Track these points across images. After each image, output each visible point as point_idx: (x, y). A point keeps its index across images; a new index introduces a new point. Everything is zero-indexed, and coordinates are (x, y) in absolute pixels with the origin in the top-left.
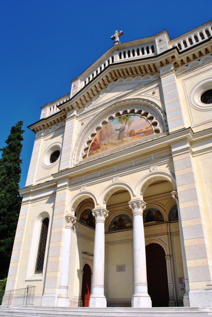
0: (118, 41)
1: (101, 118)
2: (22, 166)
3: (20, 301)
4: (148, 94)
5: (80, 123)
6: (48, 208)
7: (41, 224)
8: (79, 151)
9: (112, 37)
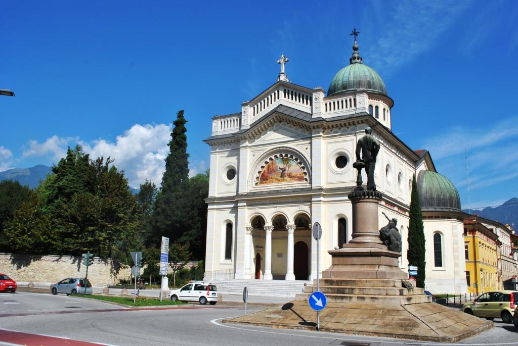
0: (283, 73)
1: (269, 155)
4: (301, 146)
5: (252, 154)
6: (232, 218)
8: (252, 179)
9: (278, 62)
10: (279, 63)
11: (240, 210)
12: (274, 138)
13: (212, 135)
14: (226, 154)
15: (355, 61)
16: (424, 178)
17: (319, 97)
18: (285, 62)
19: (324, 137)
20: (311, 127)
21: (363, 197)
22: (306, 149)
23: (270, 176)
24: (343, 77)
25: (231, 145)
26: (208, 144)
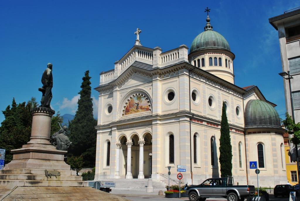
0: (138, 40)
1: (129, 95)
3: (102, 177)
4: (146, 88)
7: (107, 144)
10: (136, 34)
11: (113, 133)
12: (132, 83)
13: (100, 85)
14: (107, 96)
15: (207, 29)
16: (251, 105)
17: (157, 53)
18: (139, 32)
19: (160, 80)
20: (152, 74)
21: (37, 111)
22: (150, 89)
23: (131, 109)
24: (197, 41)
25: (106, 91)
26: (97, 90)
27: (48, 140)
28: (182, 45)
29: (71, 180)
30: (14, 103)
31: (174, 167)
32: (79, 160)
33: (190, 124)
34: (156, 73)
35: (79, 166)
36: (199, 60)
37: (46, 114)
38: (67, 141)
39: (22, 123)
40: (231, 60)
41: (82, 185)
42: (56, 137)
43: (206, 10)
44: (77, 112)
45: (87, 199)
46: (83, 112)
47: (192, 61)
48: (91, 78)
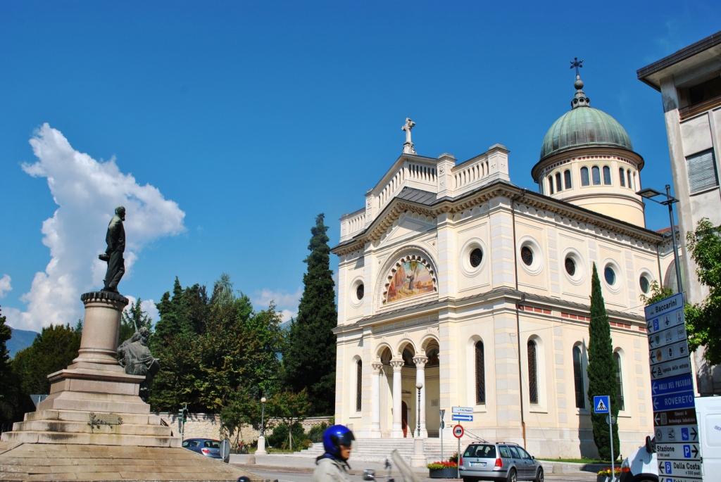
2: (334, 278)
8: (379, 295)
9: (403, 129)
10: (404, 130)
12: (399, 234)
13: (341, 242)
15: (577, 105)
17: (446, 167)
19: (453, 225)
20: (434, 213)
23: (399, 289)
27: (112, 355)
28: (494, 146)
29: (145, 433)
30: (177, 287)
31: (485, 412)
32: (300, 400)
33: (518, 315)
34: (444, 209)
35: (300, 412)
36: (558, 175)
37: (106, 305)
38: (144, 356)
39: (191, 327)
40: (633, 169)
41: (167, 445)
42: (124, 349)
43: (581, 64)
44: (302, 300)
45: (158, 471)
46: (314, 300)
47: (545, 178)
48: (328, 229)
